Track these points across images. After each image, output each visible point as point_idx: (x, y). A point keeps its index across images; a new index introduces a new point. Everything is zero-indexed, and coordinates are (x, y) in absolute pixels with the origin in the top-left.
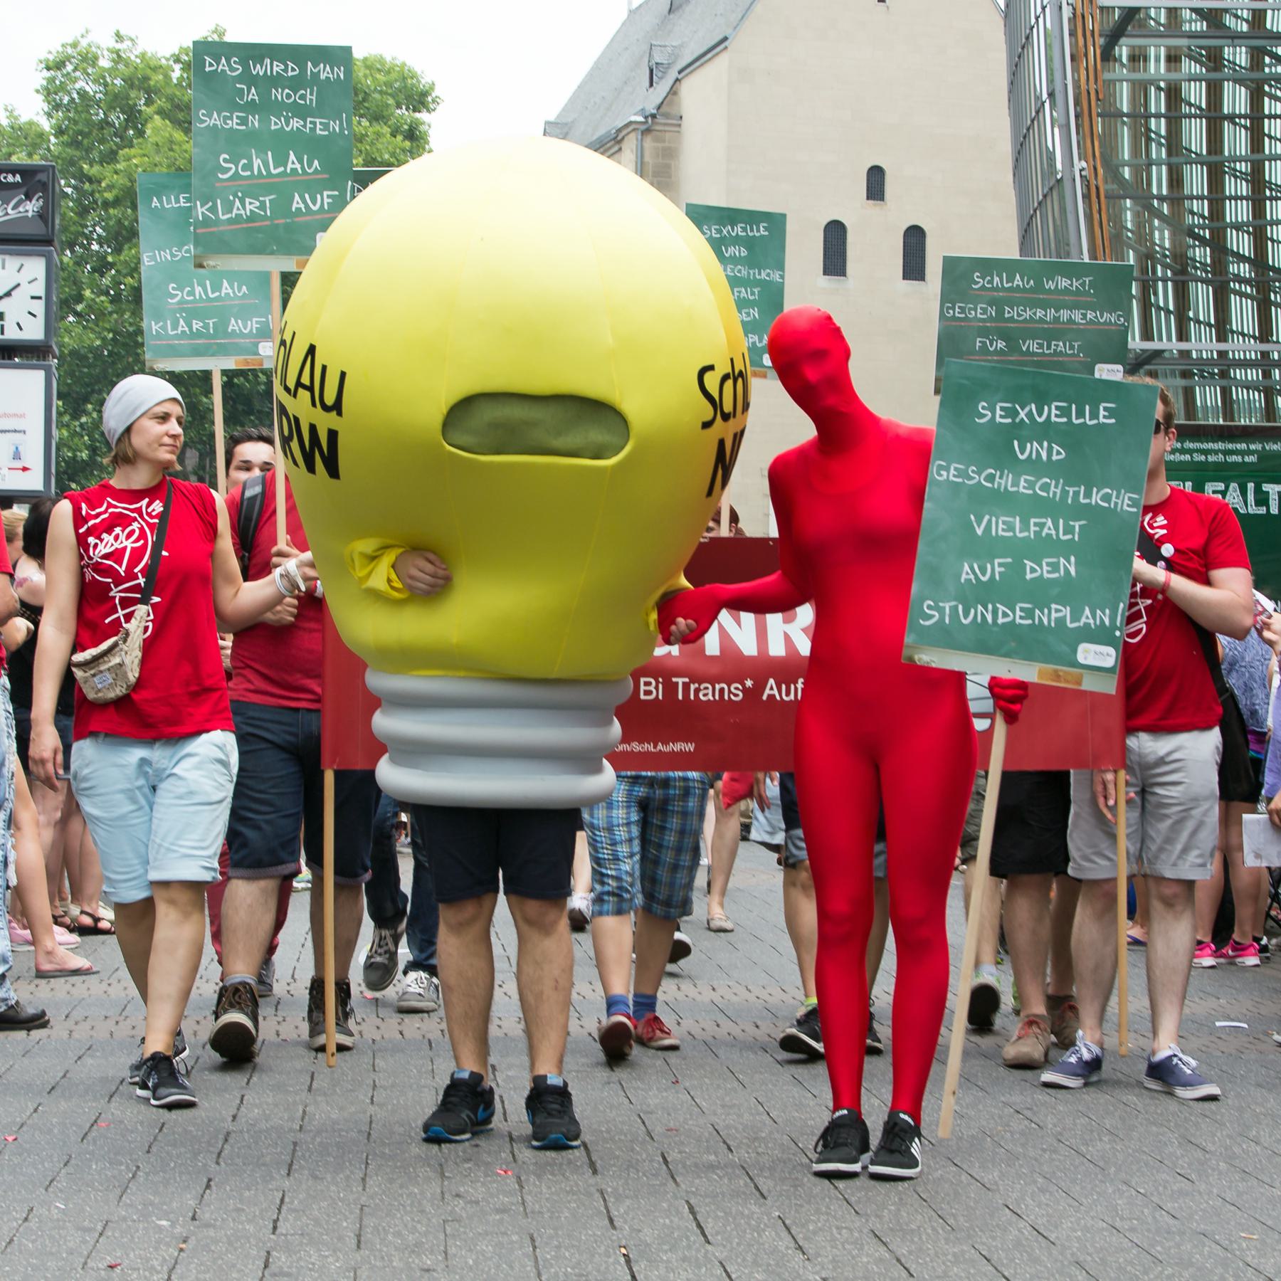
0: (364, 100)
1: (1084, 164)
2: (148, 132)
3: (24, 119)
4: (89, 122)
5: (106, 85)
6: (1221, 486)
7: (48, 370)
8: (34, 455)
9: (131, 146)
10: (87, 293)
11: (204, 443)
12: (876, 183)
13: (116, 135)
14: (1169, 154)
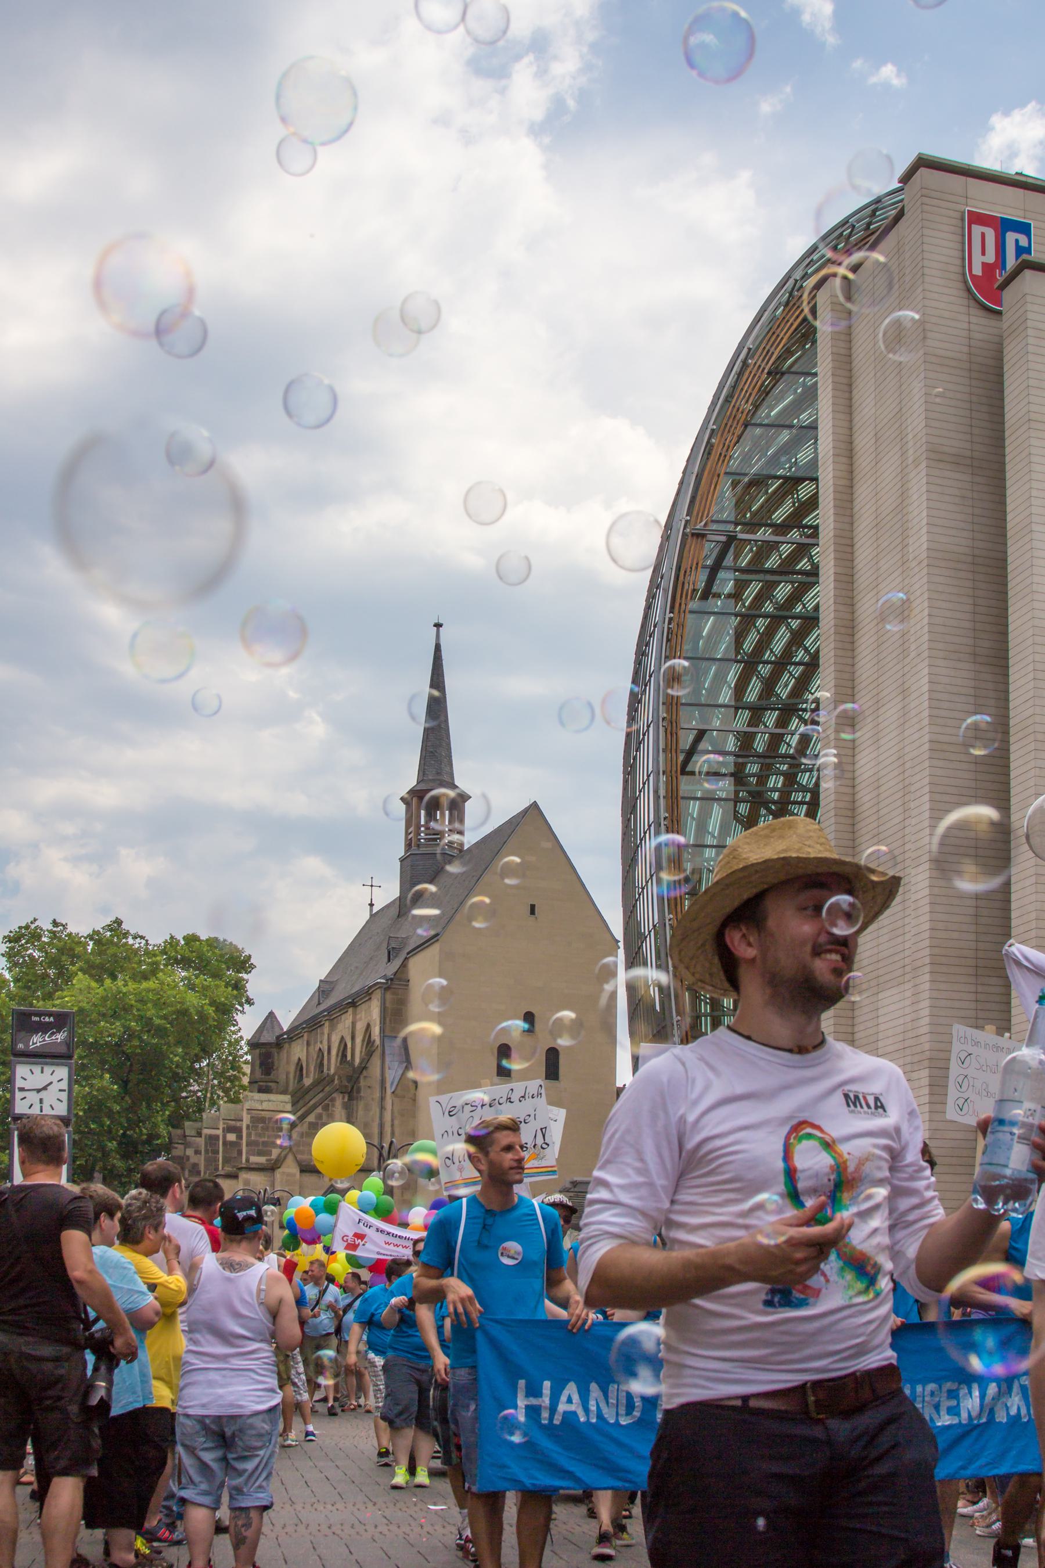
0: (207, 965)
4: (35, 975)
5: (47, 953)
9: (62, 990)
14: (712, 1009)
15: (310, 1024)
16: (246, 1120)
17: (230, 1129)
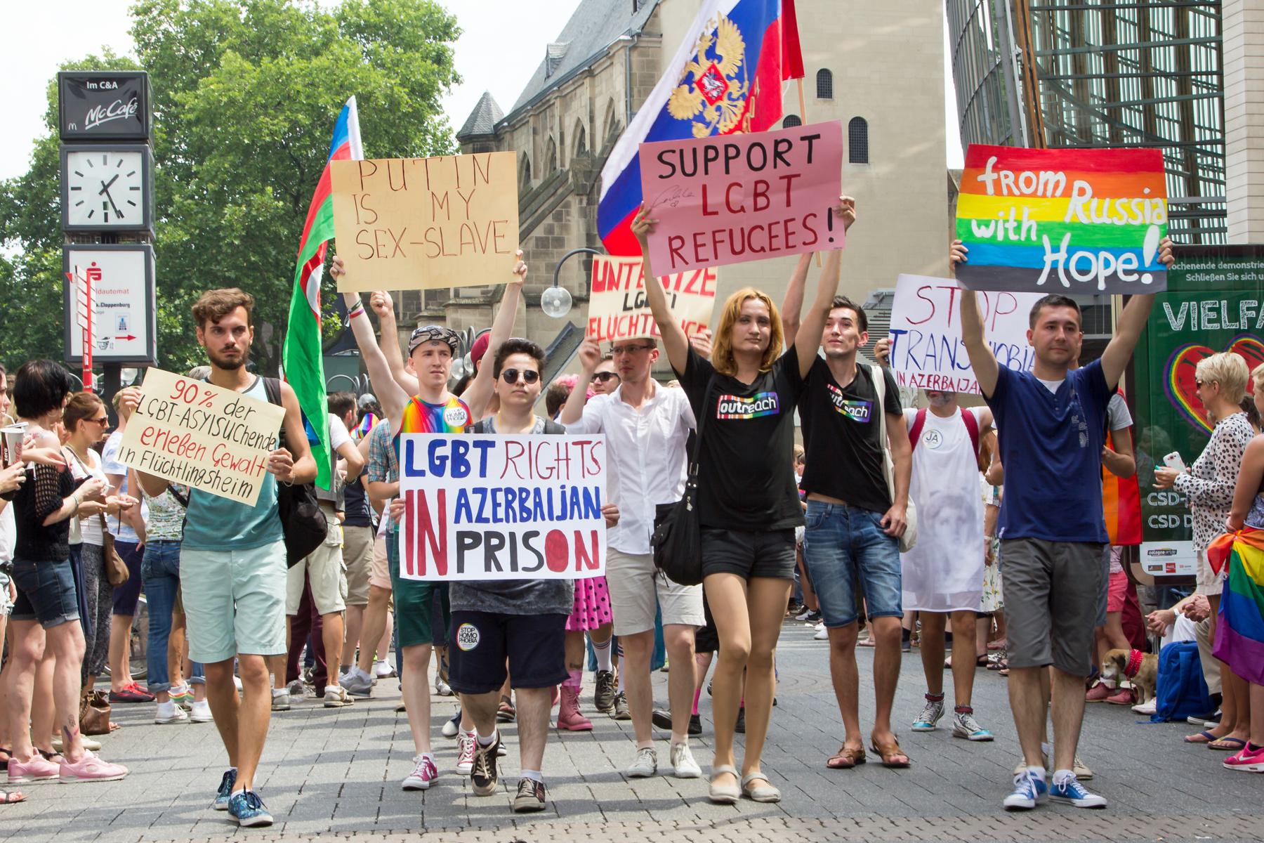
0: (398, 33)
1: (1020, 51)
2: (222, 63)
3: (119, 56)
6: (1254, 303)
7: (147, 250)
8: (138, 326)
9: (208, 75)
10: (177, 198)
11: (277, 318)
13: (195, 67)
14: (1073, 45)
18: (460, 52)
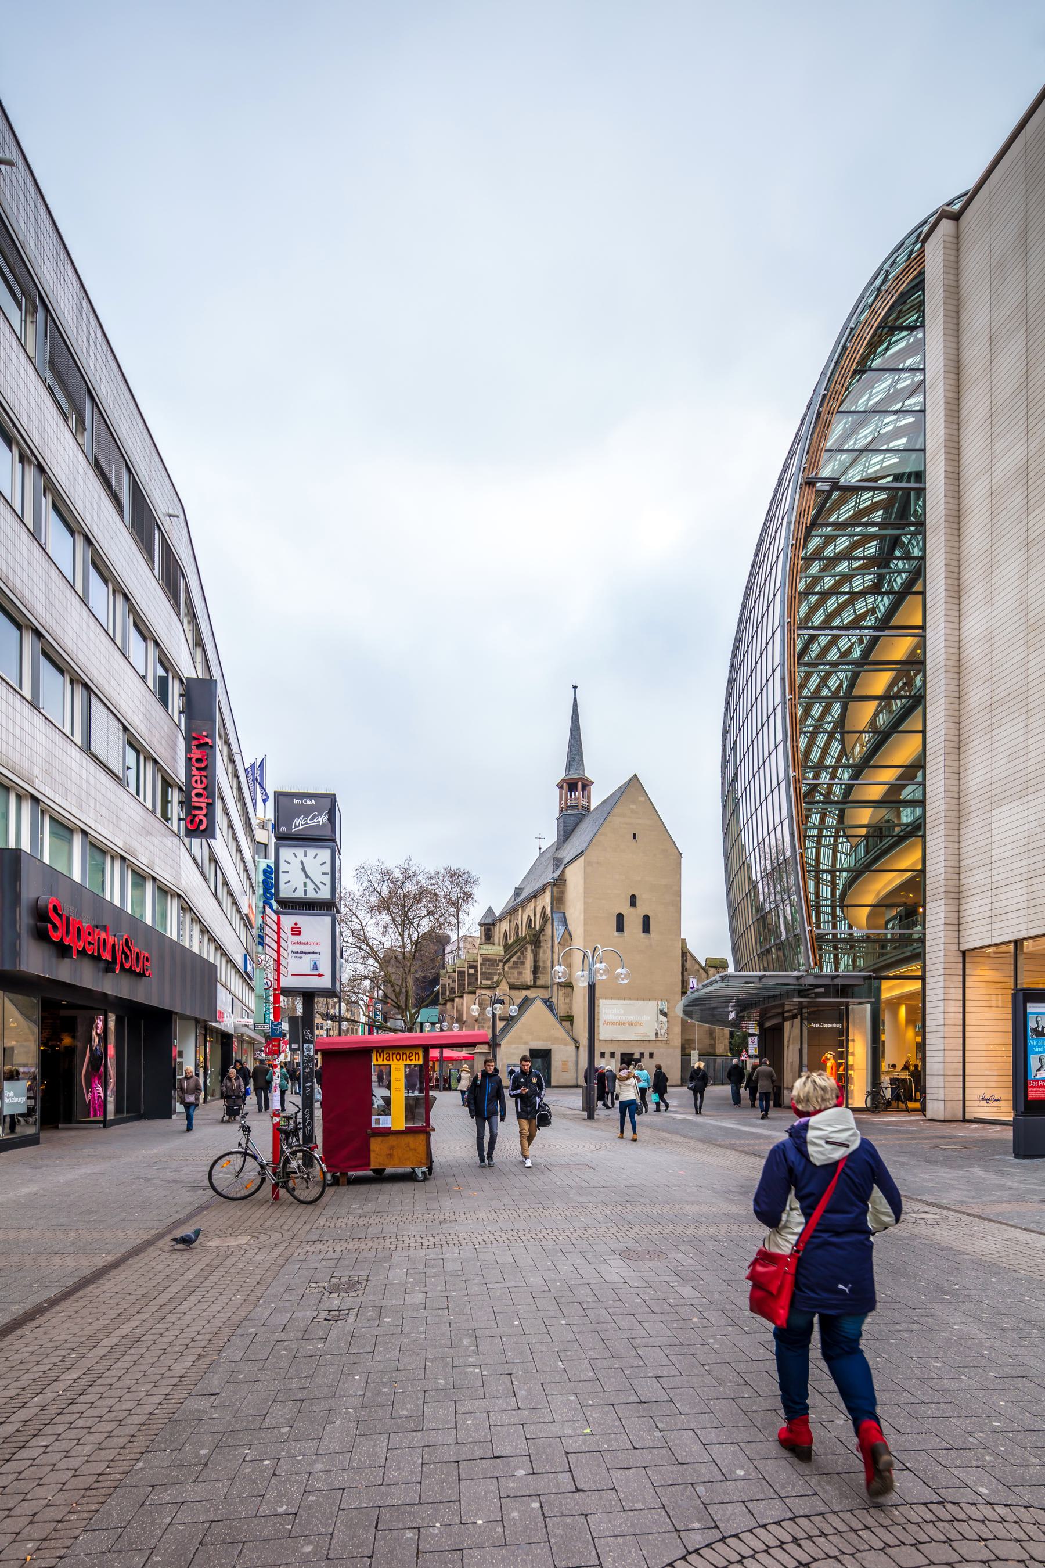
12: (633, 901)
15: (511, 912)
16: (480, 960)
17: (470, 967)
18: (478, 892)
